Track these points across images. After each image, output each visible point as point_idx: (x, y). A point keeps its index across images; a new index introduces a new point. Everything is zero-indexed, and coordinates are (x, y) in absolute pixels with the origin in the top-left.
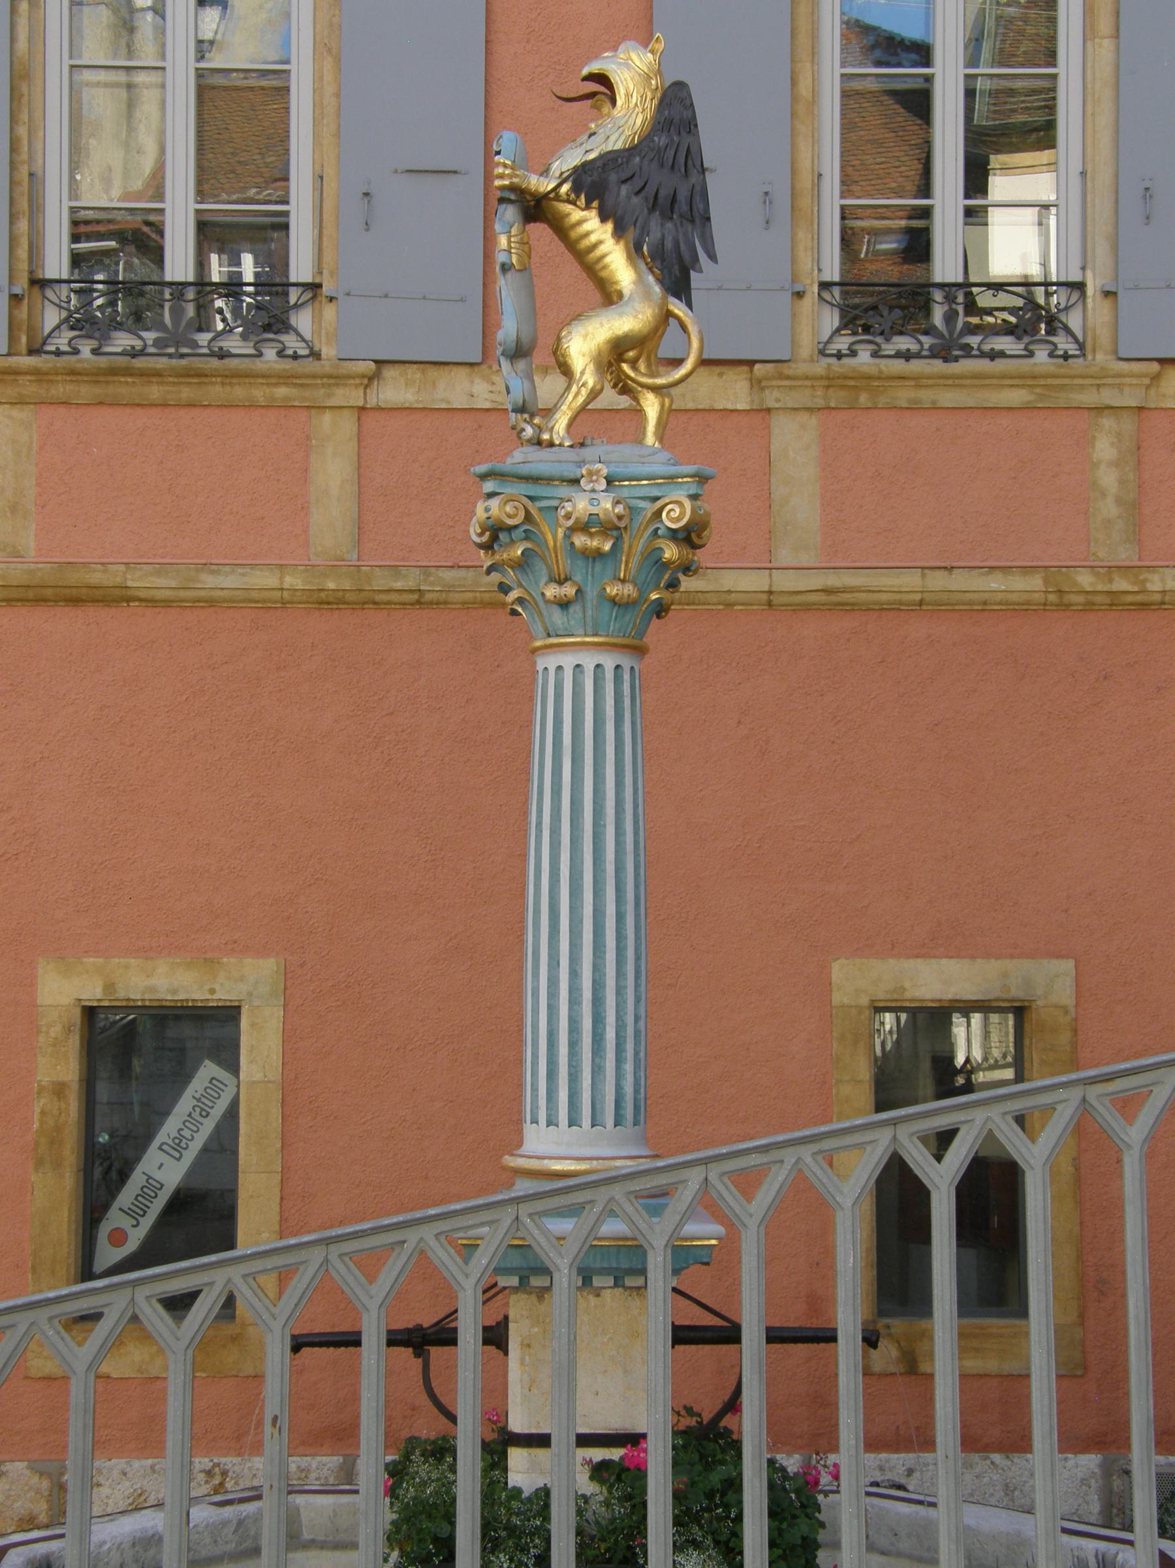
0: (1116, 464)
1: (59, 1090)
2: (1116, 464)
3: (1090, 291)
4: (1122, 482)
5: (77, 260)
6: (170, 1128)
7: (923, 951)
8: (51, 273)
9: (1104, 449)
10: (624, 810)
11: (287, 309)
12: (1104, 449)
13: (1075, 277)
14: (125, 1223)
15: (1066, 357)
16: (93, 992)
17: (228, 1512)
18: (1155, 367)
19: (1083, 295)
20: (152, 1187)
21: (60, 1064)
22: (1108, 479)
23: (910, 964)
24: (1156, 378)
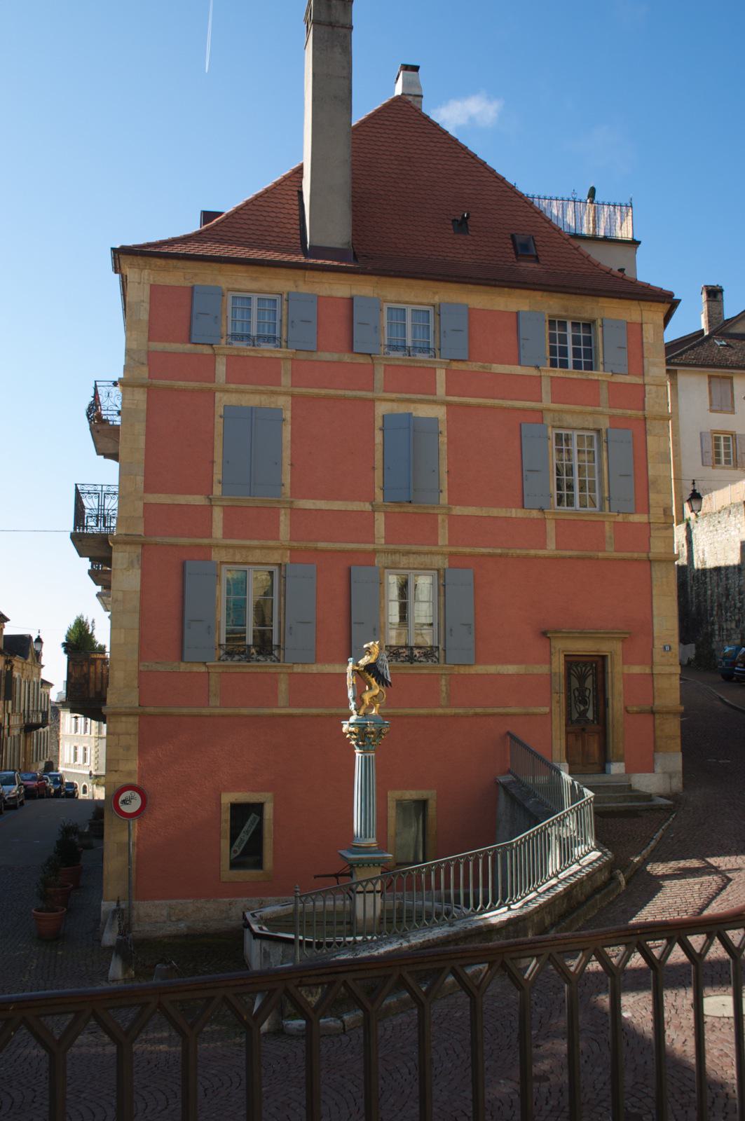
0: (446, 685)
1: (700, 944)
2: (446, 685)
3: (440, 648)
4: (447, 689)
5: (228, 639)
6: (245, 828)
7: (406, 789)
8: (222, 643)
9: (443, 682)
10: (516, 942)
11: (272, 650)
12: (443, 682)
13: (437, 645)
14: (236, 848)
15: (435, 662)
16: (233, 800)
17: (284, 907)
18: (448, 361)
19: (439, 649)
20: (242, 841)
21: (226, 816)
22: (444, 689)
23: (404, 791)
24: (449, 363)
